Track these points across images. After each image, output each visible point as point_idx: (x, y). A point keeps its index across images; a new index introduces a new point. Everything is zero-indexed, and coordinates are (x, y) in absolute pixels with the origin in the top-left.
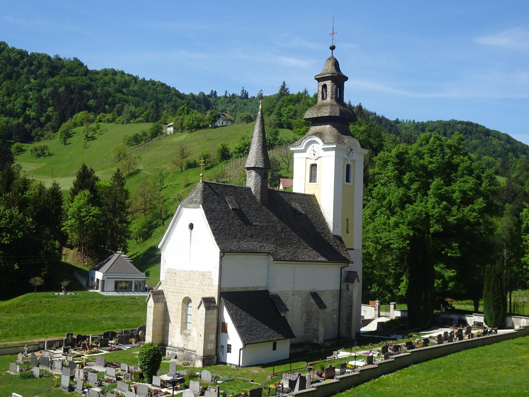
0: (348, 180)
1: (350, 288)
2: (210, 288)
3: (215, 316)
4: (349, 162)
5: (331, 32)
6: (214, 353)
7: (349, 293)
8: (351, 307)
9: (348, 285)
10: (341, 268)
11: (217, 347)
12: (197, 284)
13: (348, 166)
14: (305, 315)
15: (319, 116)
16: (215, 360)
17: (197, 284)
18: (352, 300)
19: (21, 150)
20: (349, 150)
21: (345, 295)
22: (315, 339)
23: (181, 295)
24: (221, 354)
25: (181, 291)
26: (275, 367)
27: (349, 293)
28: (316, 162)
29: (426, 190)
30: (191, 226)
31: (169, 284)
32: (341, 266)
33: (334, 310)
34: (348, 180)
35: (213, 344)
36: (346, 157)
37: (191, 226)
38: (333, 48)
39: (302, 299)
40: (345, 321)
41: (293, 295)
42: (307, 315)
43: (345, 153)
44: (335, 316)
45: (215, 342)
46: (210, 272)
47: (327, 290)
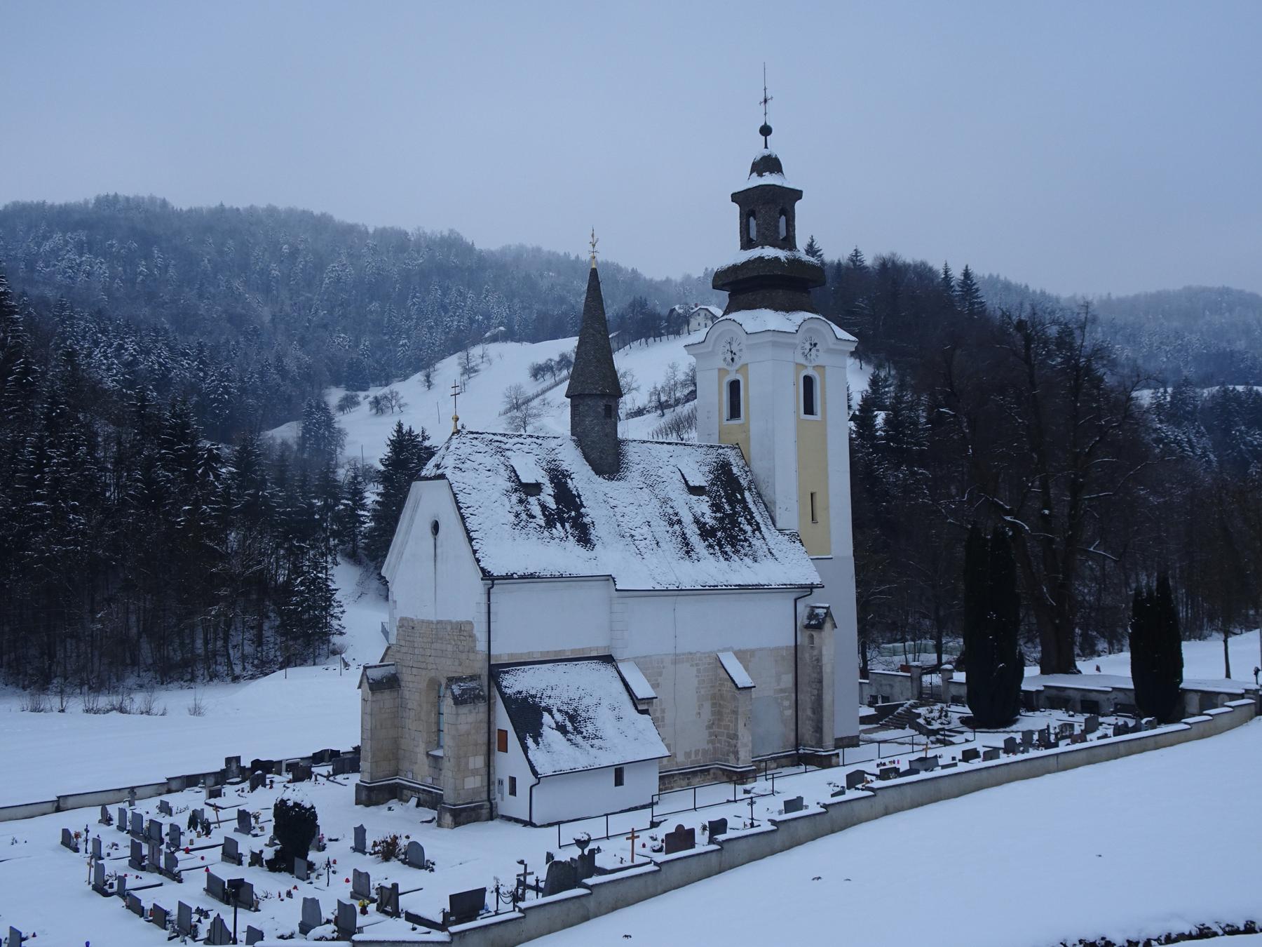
0: (809, 409)
1: (816, 640)
2: (472, 656)
3: (483, 716)
4: (810, 372)
5: (769, 102)
6: (485, 796)
7: (815, 653)
8: (820, 681)
9: (812, 637)
10: (796, 600)
11: (489, 783)
12: (450, 648)
13: (808, 382)
14: (707, 706)
15: (741, 277)
16: (485, 812)
17: (450, 648)
18: (821, 667)
19: (348, 404)
20: (808, 346)
21: (806, 656)
22: (732, 757)
23: (424, 672)
24: (498, 796)
25: (423, 665)
26: (239, 910)
27: (815, 653)
28: (739, 377)
29: (896, 416)
30: (436, 527)
31: (404, 649)
32: (795, 595)
33: (782, 691)
34: (809, 409)
35: (478, 778)
36: (802, 360)
37: (436, 527)
38: (766, 131)
39: (698, 671)
40: (809, 712)
41: (675, 662)
42: (714, 705)
43: (799, 351)
44: (786, 703)
45: (484, 771)
46: (470, 623)
47: (761, 649)
